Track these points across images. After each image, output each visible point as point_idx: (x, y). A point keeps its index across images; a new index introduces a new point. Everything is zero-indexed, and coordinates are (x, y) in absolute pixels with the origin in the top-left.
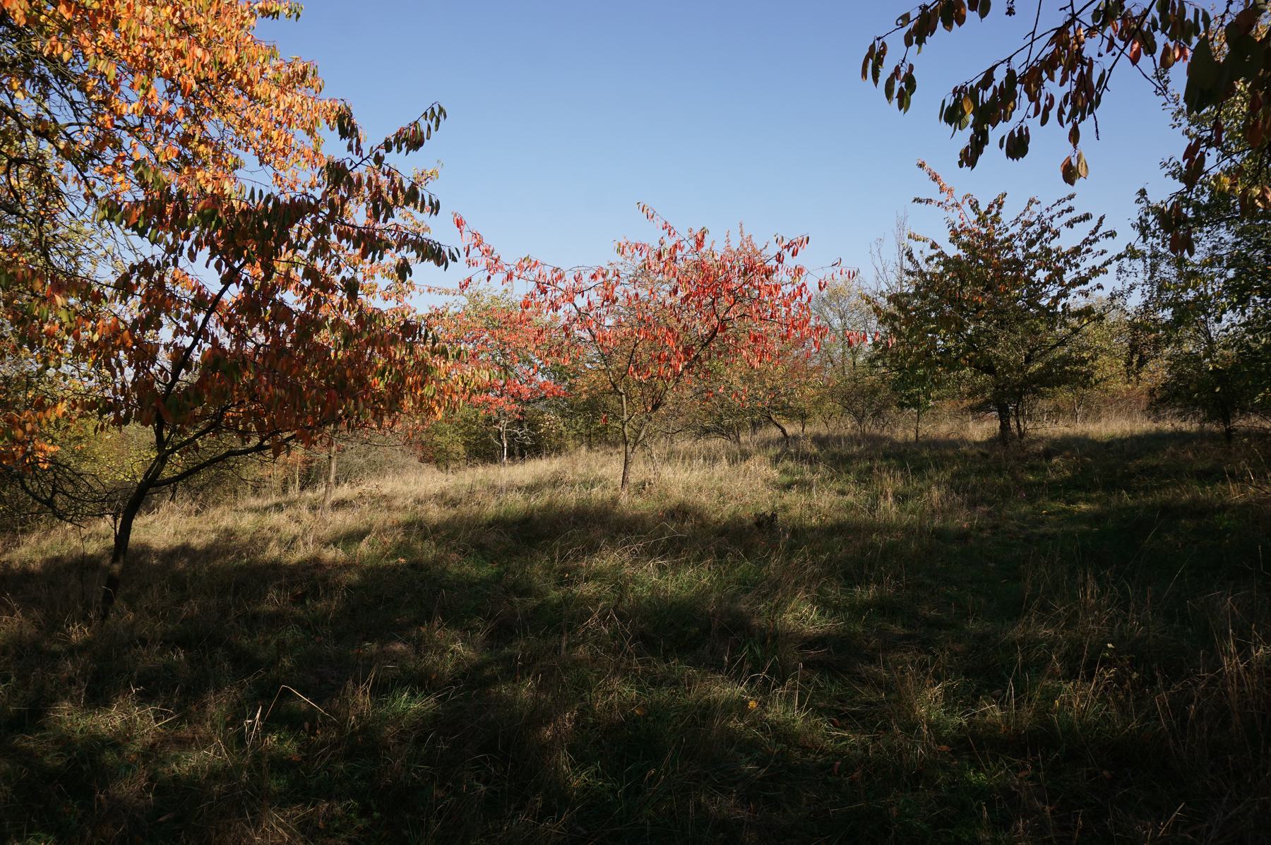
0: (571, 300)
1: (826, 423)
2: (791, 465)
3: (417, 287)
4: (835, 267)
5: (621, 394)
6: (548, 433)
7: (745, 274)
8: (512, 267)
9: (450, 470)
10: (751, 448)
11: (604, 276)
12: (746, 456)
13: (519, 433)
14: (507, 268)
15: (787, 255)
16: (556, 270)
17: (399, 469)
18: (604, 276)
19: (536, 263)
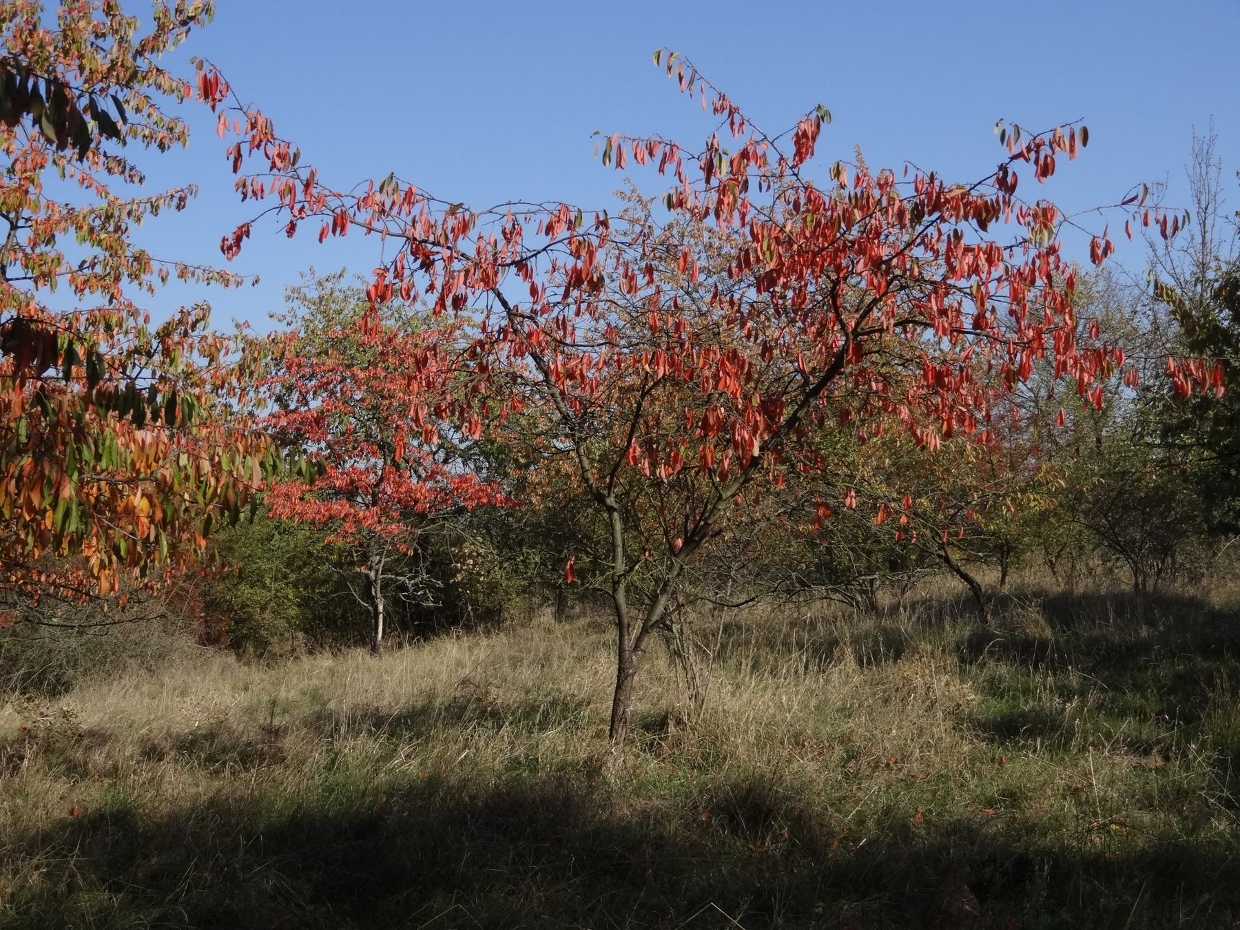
0: (488, 282)
1: (1052, 565)
2: (1003, 670)
3: (155, 266)
4: (1132, 208)
5: (610, 510)
6: (472, 580)
7: (917, 216)
8: (349, 202)
9: (1068, 272)
10: (905, 624)
11: (571, 225)
12: (896, 647)
13: (410, 584)
14: (334, 203)
15: (1025, 171)
16: (453, 210)
17: (153, 663)
18: (571, 225)
19: (409, 193)
